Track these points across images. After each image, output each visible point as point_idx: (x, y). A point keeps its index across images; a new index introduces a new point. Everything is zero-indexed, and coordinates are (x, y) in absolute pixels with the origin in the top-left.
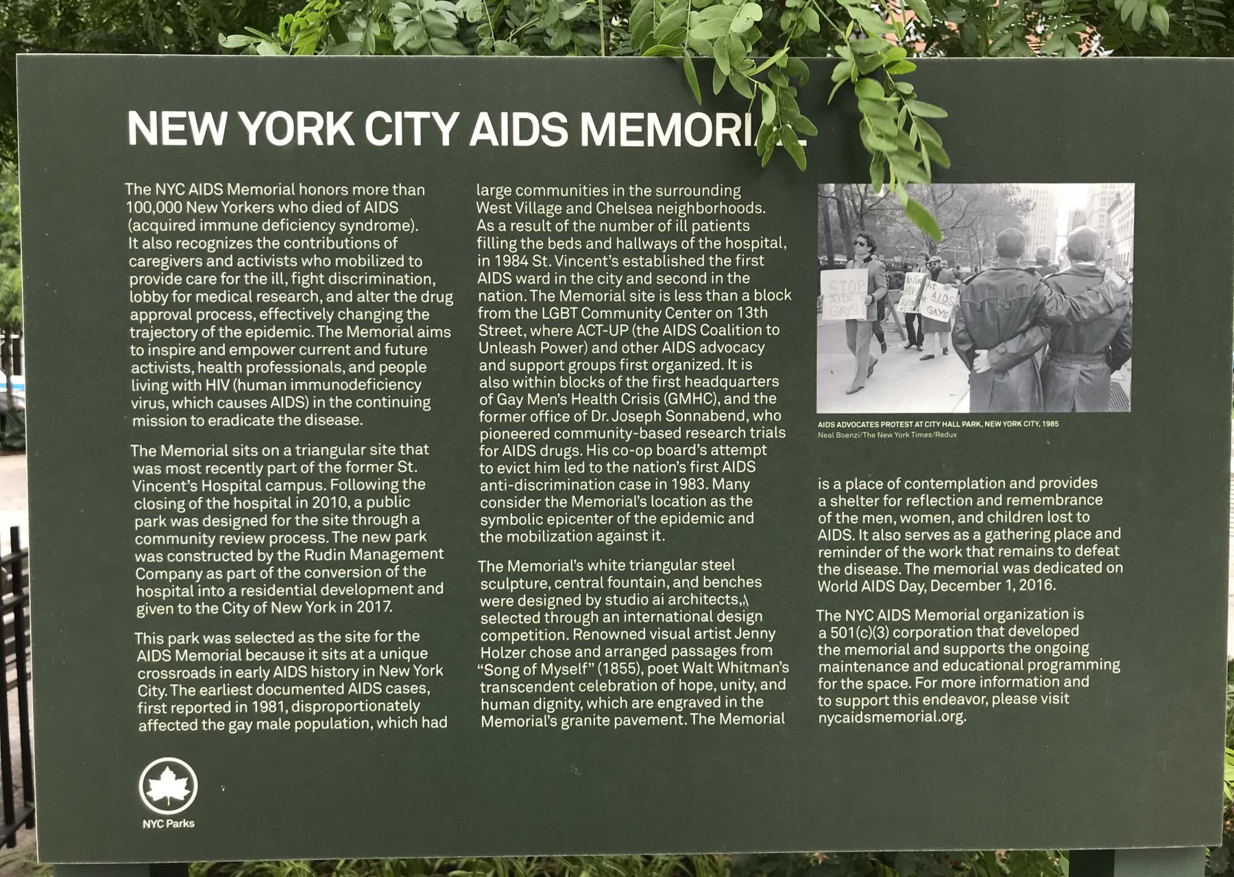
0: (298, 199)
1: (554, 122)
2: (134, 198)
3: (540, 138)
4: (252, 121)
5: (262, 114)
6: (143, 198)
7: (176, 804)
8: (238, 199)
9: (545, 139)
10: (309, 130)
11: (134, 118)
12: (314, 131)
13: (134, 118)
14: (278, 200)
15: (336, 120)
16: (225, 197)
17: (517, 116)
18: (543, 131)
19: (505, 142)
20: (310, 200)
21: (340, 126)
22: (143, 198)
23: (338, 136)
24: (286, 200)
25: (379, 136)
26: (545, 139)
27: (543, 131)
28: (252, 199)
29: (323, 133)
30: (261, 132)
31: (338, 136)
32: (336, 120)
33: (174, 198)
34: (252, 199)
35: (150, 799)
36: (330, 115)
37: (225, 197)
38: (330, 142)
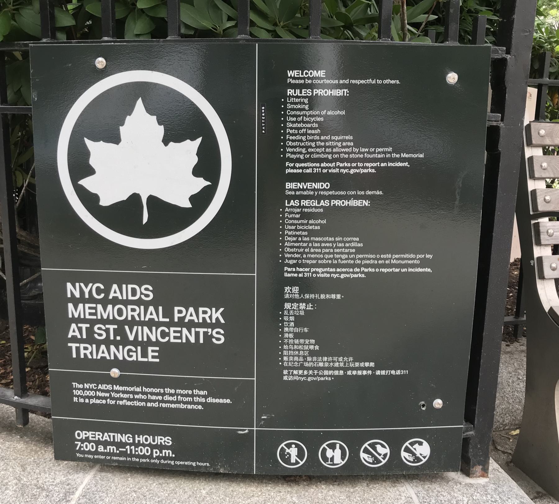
0: (143, 393)
1: (146, 289)
2: (76, 389)
3: (140, 297)
4: (86, 287)
5: (91, 285)
6: (79, 389)
7: (166, 217)
8: (118, 392)
9: (143, 297)
10: (204, 316)
11: (69, 286)
12: (207, 316)
13: (69, 286)
14: (134, 393)
15: (216, 312)
16: (113, 391)
17: (130, 286)
18: (141, 293)
19: (125, 298)
20: (146, 394)
21: (218, 314)
22: (79, 389)
23: (217, 319)
24: (138, 393)
25: (98, 294)
26: (143, 297)
27: (141, 293)
28: (124, 392)
29: (210, 317)
30: (90, 292)
31: (217, 319)
32: (216, 312)
33: (92, 390)
34: (124, 392)
35: (90, 200)
36: (214, 309)
37: (113, 391)
38: (214, 321)
